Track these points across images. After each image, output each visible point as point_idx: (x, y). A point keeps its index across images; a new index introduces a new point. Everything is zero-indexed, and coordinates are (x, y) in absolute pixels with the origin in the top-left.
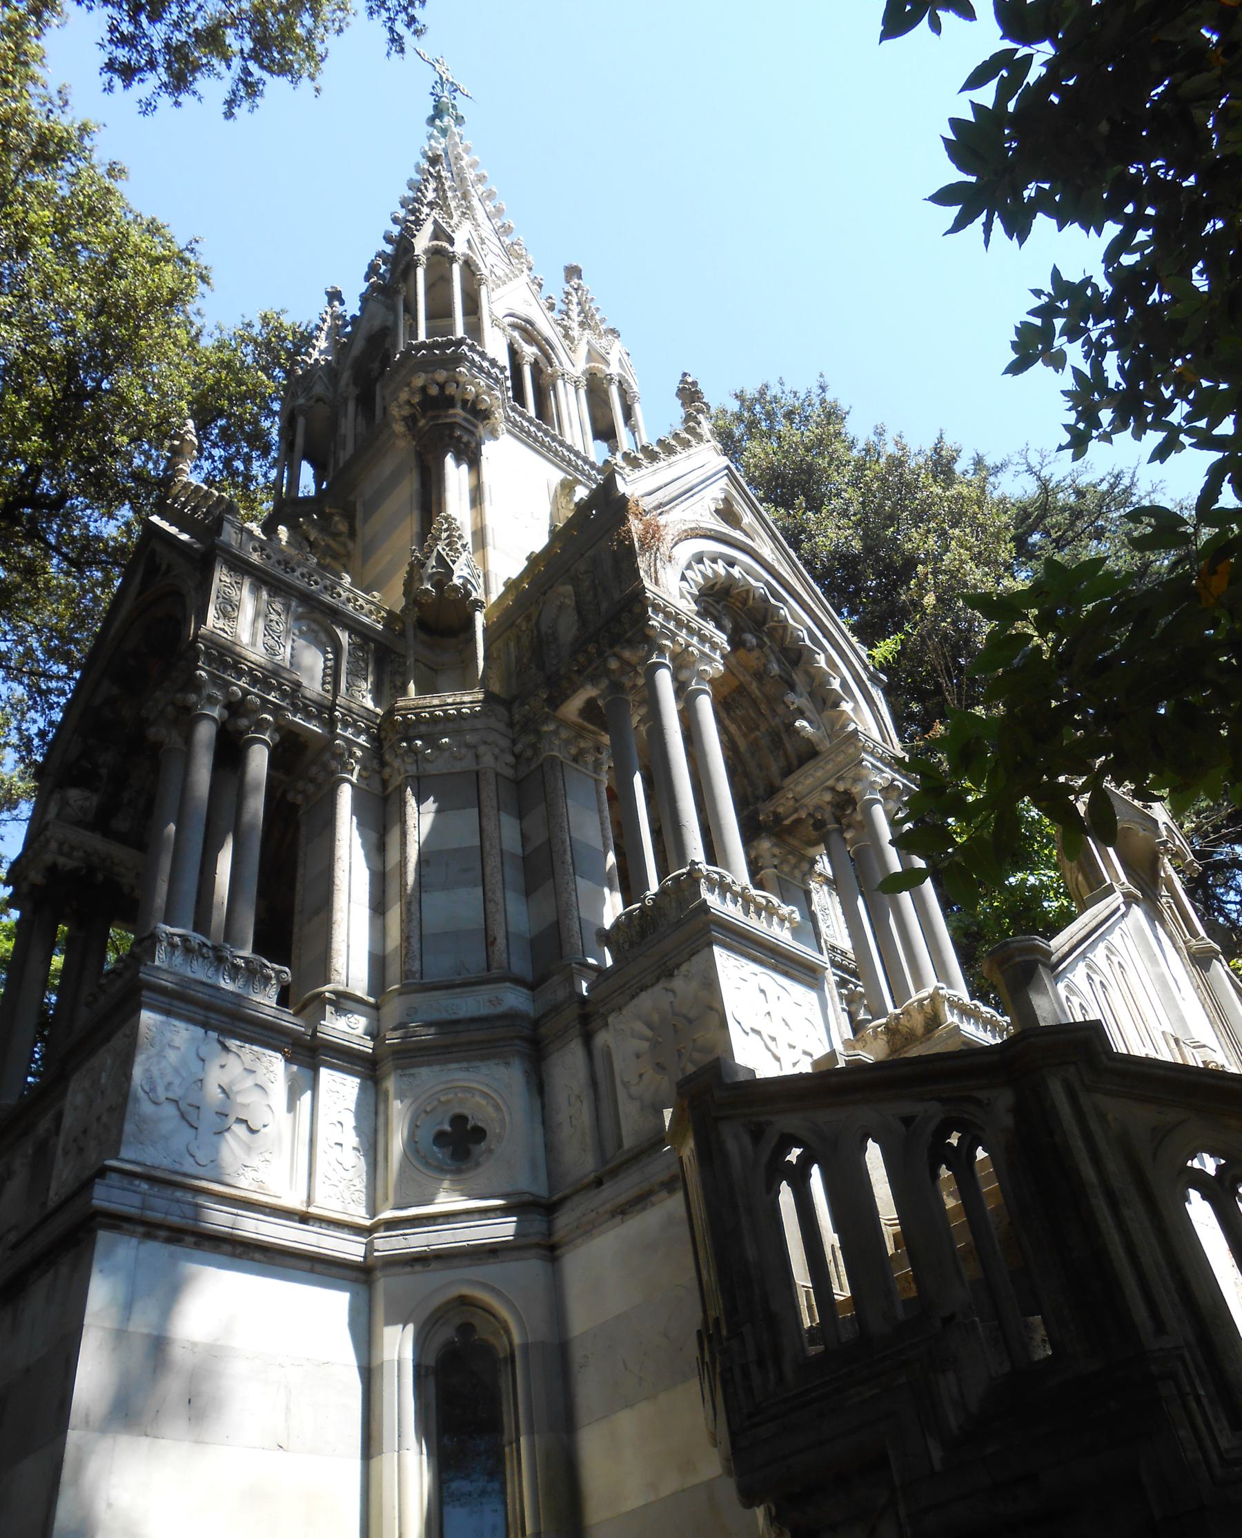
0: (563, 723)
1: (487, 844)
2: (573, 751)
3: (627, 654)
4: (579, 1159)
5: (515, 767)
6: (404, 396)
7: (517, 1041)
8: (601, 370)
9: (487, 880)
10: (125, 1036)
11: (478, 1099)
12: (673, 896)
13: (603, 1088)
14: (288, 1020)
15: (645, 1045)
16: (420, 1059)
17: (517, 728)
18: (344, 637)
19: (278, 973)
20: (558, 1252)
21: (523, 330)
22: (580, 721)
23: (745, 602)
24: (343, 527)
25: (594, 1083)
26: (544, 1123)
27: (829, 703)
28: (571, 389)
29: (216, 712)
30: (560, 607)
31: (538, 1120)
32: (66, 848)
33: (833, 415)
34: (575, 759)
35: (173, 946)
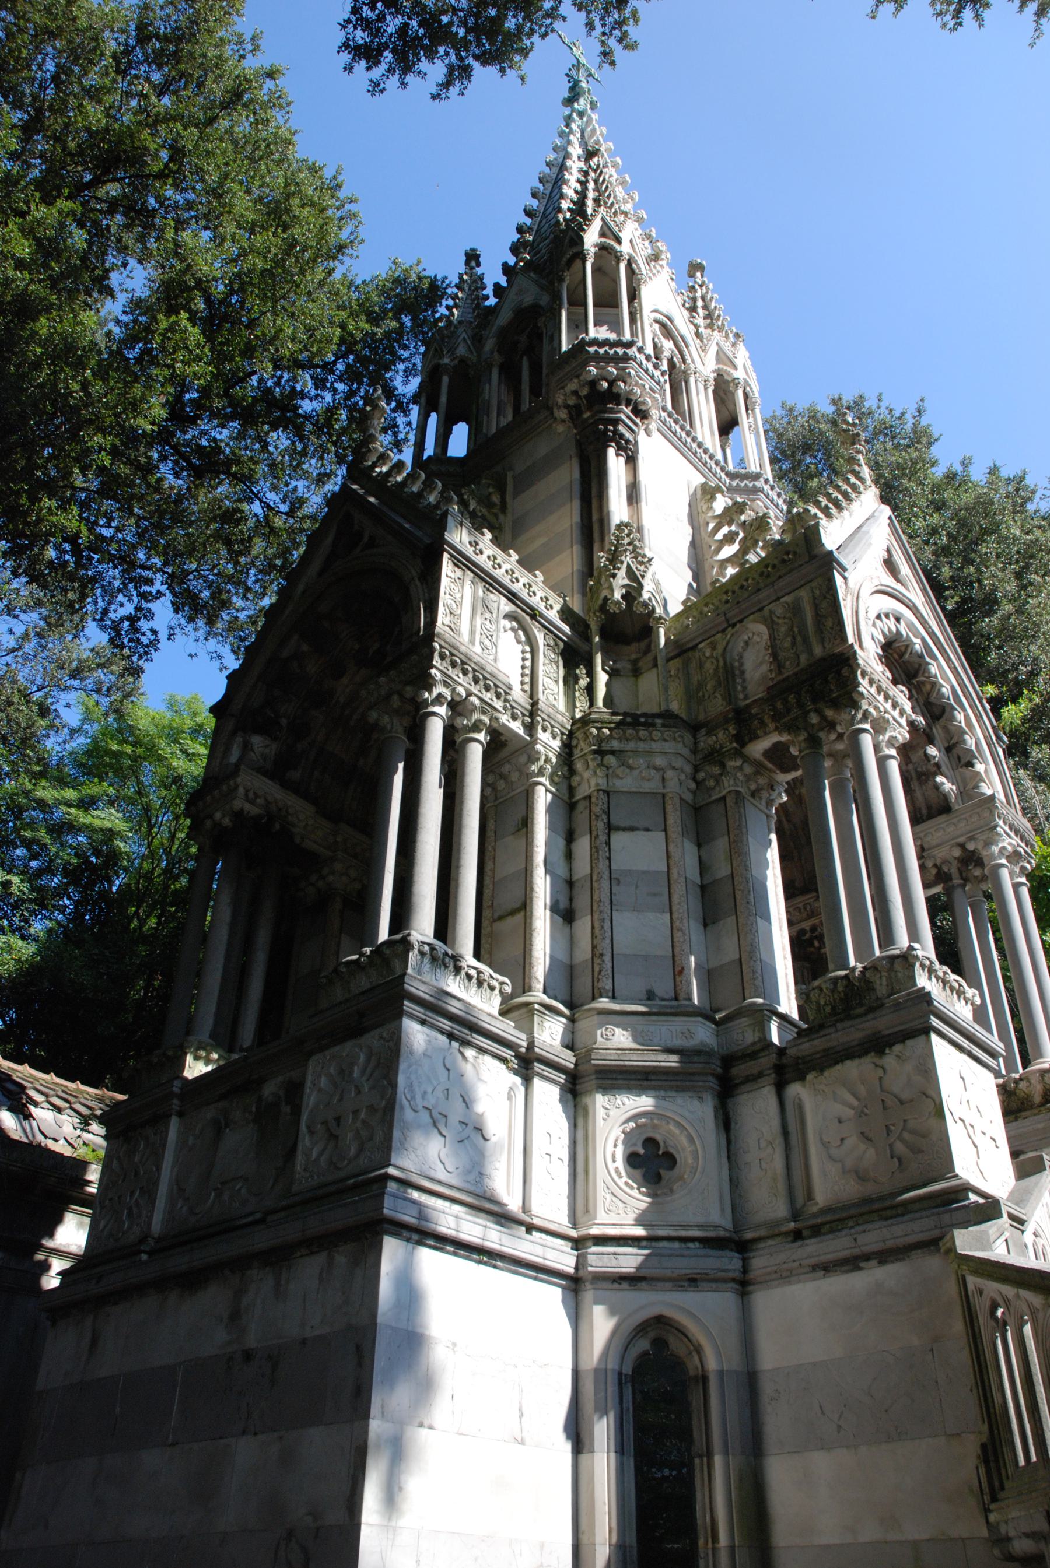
0: (746, 759)
1: (674, 872)
2: (753, 787)
3: (829, 713)
4: (769, 1204)
5: (694, 793)
6: (572, 386)
7: (711, 1078)
8: (729, 374)
9: (674, 909)
10: (381, 1037)
11: (672, 1127)
12: (884, 974)
13: (794, 1139)
14: (506, 1028)
15: (850, 1113)
16: (620, 1082)
17: (700, 756)
18: (540, 636)
19: (502, 983)
20: (750, 1288)
21: (663, 325)
22: (762, 759)
23: (902, 655)
24: (496, 499)
25: (785, 1133)
26: (729, 1157)
27: (963, 761)
28: (701, 388)
29: (481, 736)
30: (747, 643)
31: (724, 1154)
32: (251, 795)
33: (921, 438)
34: (753, 795)
35: (422, 953)
